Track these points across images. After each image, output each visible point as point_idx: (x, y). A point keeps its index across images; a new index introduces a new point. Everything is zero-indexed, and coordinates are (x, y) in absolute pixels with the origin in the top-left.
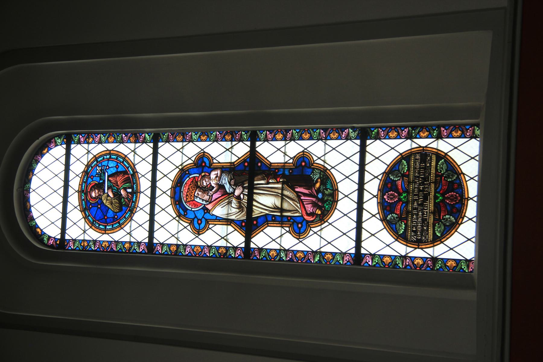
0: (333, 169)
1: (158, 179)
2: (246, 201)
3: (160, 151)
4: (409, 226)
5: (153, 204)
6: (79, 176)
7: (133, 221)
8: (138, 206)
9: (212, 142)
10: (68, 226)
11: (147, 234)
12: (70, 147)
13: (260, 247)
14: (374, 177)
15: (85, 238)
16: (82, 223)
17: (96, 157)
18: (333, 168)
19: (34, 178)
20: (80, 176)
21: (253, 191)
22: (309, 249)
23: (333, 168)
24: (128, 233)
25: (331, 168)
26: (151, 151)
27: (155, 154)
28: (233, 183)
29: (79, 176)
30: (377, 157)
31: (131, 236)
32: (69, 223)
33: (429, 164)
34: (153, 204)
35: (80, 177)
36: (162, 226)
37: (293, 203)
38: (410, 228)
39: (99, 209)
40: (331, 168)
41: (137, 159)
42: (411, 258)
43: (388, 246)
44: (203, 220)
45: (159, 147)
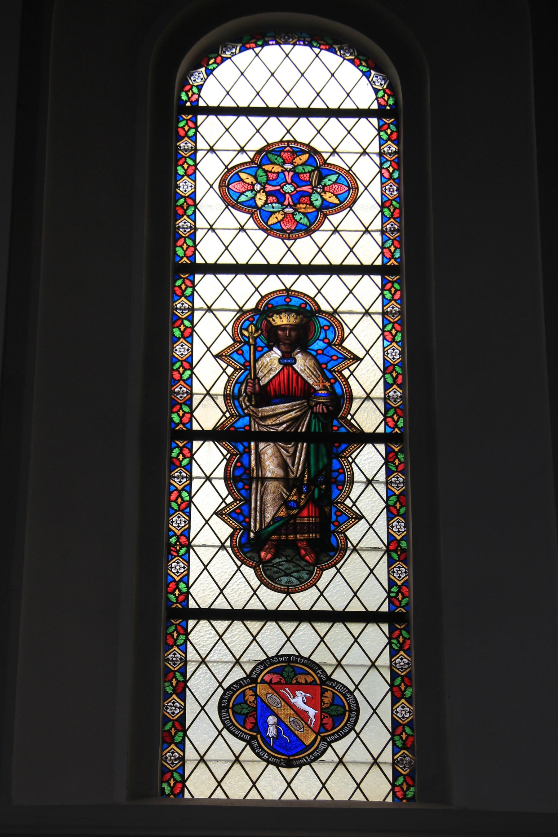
0: (355, 735)
7: (239, 766)
8: (350, 496)
10: (352, 106)
12: (373, 117)
14: (324, 782)
17: (228, 169)
18: (358, 735)
20: (317, 50)
21: (312, 432)
23: (358, 735)
24: (211, 226)
25: (358, 732)
27: (219, 111)
28: (318, 410)
31: (365, 400)
33: (311, 488)
37: (295, 387)
38: (229, 421)
40: (358, 732)
41: (323, 770)
42: (385, 324)
44: (176, 656)
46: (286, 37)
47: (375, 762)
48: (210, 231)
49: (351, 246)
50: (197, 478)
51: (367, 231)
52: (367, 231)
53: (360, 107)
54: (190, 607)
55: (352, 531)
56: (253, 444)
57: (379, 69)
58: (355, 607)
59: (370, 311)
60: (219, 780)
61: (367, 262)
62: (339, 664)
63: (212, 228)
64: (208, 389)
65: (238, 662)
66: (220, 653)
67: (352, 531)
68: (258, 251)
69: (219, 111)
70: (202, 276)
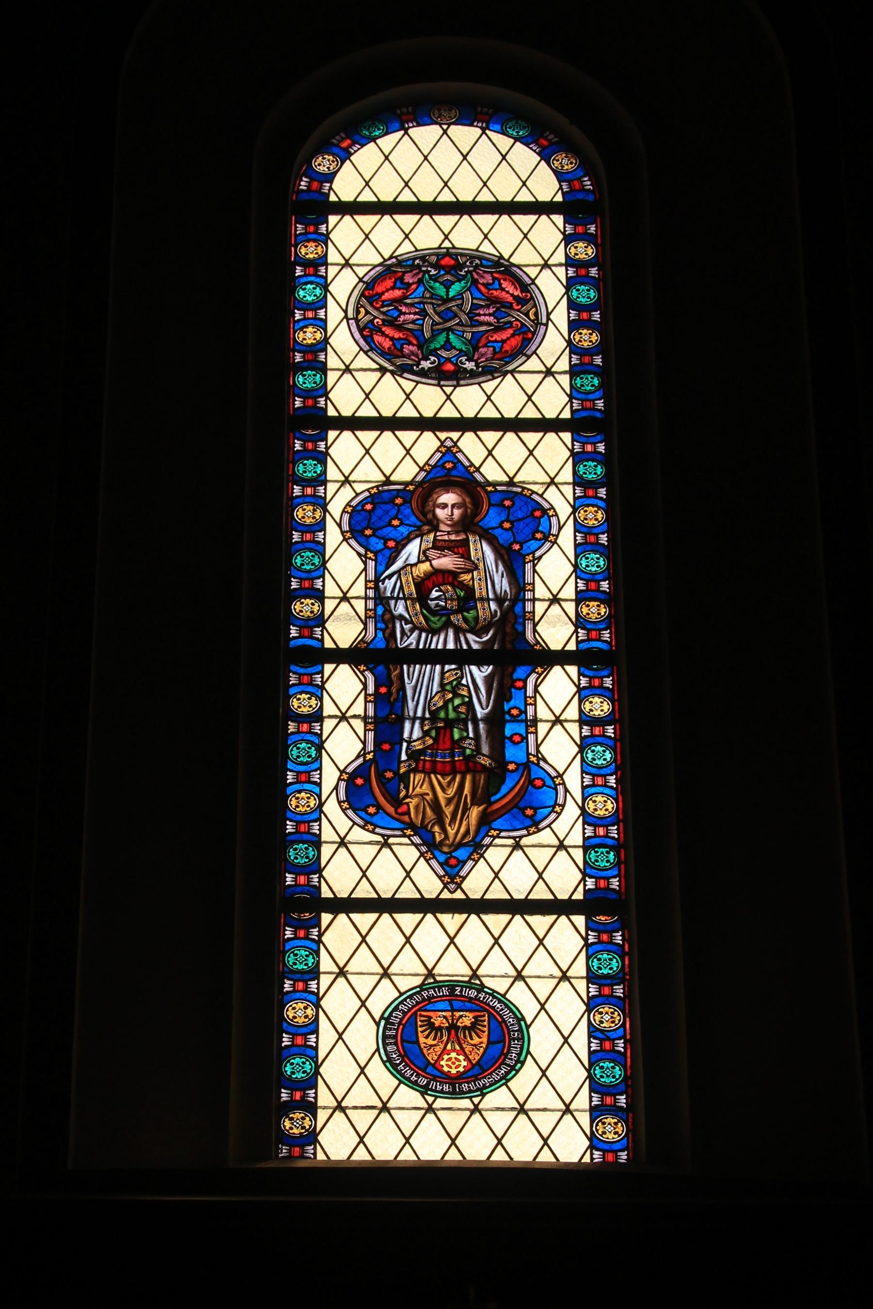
1: (482, 434)
2: (429, 667)
3: (551, 436)
4: (597, 888)
5: (421, 424)
6: (451, 393)
9: (573, 562)
11: (346, 412)
13: (319, 1138)
15: (324, 844)
16: (369, 257)
19: (476, 131)
20: (486, 248)
22: (323, 1122)
26: (551, 414)
27: (354, 424)
29: (451, 393)
30: (359, 1071)
32: (367, 221)
34: (421, 424)
35: (480, 249)
36: (367, 452)
39: (378, 533)
43: (465, 157)
45: (561, 434)
46: (449, 466)
47: (567, 1110)
48: (337, 1112)
49: (530, 393)
50: (330, 717)
51: (564, 977)
52: (564, 977)
53: (540, 199)
54: (323, 896)
55: (524, 150)
56: (405, 667)
57: (568, 146)
58: (530, 413)
59: (561, 718)
60: (364, 869)
61: (550, 413)
62: (519, 976)
63: (340, 1107)
64: (347, 475)
65: (386, 974)
66: (363, 961)
67: (524, 150)
68: (408, 401)
69: (354, 424)
70: (337, 432)
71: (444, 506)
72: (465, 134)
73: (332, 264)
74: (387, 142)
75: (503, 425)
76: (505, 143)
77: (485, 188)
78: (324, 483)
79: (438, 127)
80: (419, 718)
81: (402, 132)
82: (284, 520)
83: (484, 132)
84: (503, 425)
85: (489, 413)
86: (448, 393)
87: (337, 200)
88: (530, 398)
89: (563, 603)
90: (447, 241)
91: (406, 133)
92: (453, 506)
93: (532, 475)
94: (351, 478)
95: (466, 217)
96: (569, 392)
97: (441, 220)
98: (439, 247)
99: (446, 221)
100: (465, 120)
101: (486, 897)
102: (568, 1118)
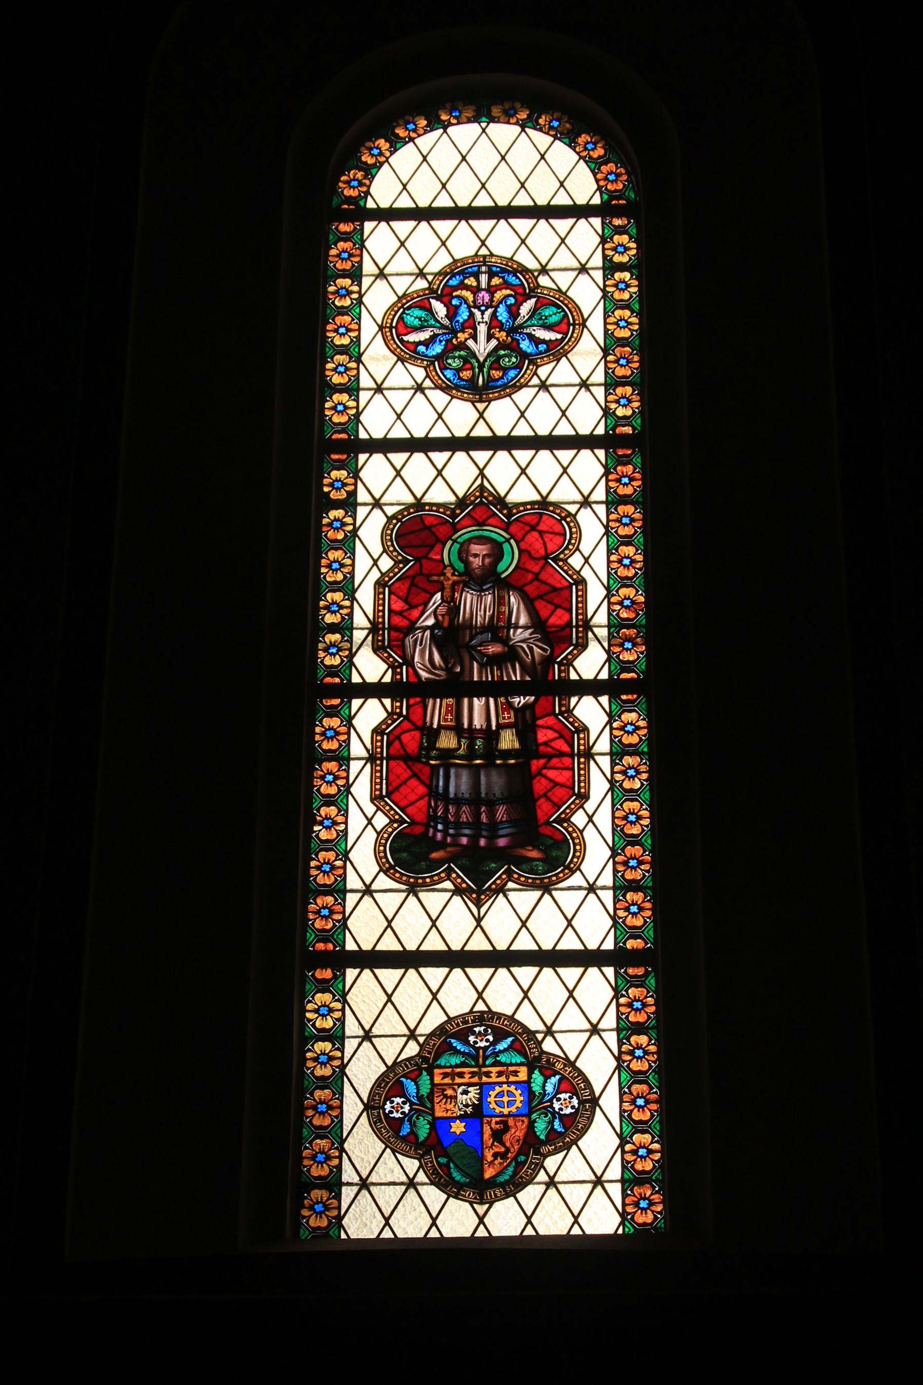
16: (399, 495)
32: (403, 227)
47: (595, 1030)
58: (565, 455)
70: (361, 700)
71: (476, 556)
72: (504, 132)
73: (364, 389)
74: (425, 141)
75: (536, 443)
76: (542, 140)
77: (523, 189)
78: (344, 891)
79: (476, 125)
80: (452, 540)
81: (441, 131)
82: (317, 408)
83: (523, 130)
84: (536, 443)
85: (522, 430)
86: (481, 410)
87: (376, 207)
88: (565, 471)
89: (594, 506)
90: (484, 248)
91: (445, 131)
92: (484, 556)
93: (564, 494)
94: (386, 271)
95: (502, 222)
96: (604, 462)
97: (478, 224)
98: (476, 255)
99: (483, 226)
100: (507, 117)
101: (512, 948)
102: (595, 1038)
